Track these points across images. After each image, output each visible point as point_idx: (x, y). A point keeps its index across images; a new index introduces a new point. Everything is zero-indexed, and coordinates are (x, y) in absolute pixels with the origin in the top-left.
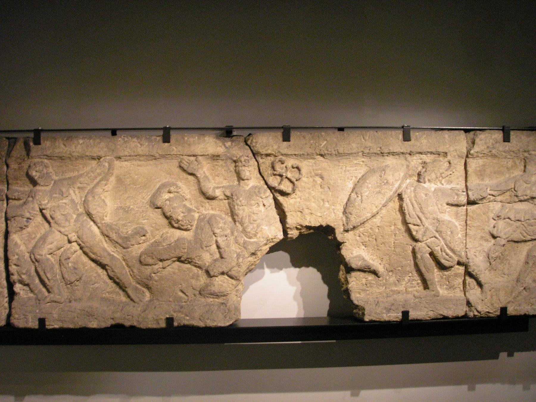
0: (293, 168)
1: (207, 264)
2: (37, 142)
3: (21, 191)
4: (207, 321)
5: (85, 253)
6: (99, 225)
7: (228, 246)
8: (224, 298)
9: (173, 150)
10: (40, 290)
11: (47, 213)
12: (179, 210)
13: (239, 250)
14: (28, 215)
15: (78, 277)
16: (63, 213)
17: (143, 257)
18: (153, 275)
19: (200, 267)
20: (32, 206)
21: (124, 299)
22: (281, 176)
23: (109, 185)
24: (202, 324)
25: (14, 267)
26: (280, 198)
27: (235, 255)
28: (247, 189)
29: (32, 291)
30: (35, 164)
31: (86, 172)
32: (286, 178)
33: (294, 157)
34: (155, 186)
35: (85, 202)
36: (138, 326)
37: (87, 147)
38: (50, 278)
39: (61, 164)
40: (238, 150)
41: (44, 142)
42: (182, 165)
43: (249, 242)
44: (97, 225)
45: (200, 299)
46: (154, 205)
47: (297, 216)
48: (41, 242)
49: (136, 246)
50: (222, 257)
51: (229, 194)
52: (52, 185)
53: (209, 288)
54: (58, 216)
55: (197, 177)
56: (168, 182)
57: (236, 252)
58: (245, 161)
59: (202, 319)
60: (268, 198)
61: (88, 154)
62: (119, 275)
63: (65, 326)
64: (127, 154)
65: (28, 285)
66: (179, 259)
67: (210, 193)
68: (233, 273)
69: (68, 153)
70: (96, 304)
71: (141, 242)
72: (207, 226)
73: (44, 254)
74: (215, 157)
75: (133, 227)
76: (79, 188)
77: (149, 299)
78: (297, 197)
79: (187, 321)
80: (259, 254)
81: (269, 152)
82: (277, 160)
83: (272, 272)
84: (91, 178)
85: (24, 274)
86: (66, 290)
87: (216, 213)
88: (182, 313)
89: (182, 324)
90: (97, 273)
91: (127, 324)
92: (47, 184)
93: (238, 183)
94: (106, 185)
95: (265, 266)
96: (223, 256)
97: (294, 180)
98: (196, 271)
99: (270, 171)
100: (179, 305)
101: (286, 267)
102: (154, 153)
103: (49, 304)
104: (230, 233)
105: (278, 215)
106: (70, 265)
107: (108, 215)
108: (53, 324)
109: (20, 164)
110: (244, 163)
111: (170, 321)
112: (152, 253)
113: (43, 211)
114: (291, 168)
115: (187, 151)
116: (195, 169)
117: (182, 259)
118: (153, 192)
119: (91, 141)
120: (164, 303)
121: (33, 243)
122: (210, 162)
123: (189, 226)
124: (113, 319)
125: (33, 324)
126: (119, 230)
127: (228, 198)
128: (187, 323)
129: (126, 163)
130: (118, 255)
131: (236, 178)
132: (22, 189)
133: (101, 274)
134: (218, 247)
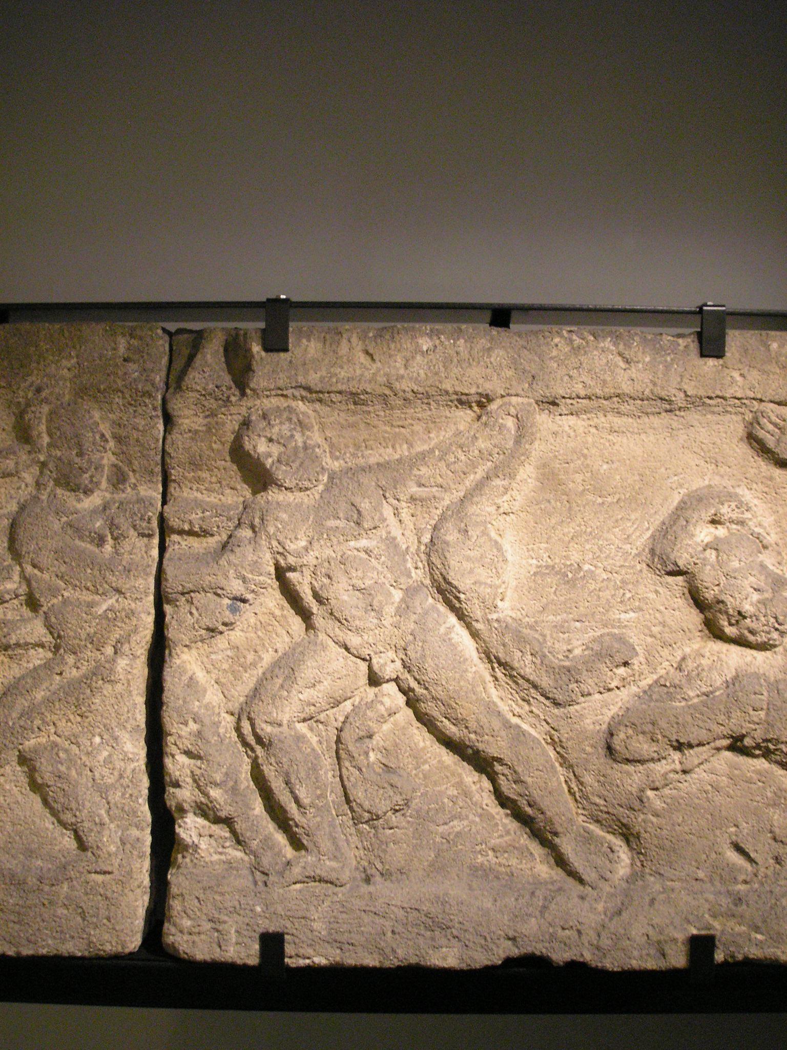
2: (276, 342)
3: (215, 507)
5: (424, 719)
9: (733, 381)
10: (267, 838)
11: (302, 582)
14: (236, 587)
16: (360, 584)
18: (650, 793)
20: (251, 557)
21: (544, 869)
25: (182, 759)
29: (239, 841)
30: (264, 416)
31: (437, 447)
34: (666, 499)
37: (447, 362)
38: (306, 801)
39: (352, 419)
41: (298, 344)
42: (761, 434)
44: (468, 626)
46: (664, 564)
48: (279, 681)
49: (597, 696)
52: (321, 488)
54: (341, 593)
56: (710, 486)
61: (447, 386)
62: (536, 794)
63: (351, 960)
64: (579, 389)
65: (227, 822)
66: (737, 745)
69: (382, 379)
70: (455, 889)
71: (613, 685)
73: (285, 718)
76: (413, 499)
85: (216, 785)
86: (354, 840)
88: (741, 919)
89: (740, 957)
90: (460, 784)
91: (560, 956)
92: (307, 484)
103: (298, 886)
106: (372, 756)
107: (509, 593)
108: (310, 951)
109: (213, 414)
111: (701, 945)
113: (290, 575)
117: (748, 742)
118: (659, 518)
119: (461, 342)
120: (677, 884)
121: (249, 680)
123: (775, 635)
124: (513, 939)
125: (243, 951)
128: (755, 953)
129: (572, 420)
130: (534, 726)
132: (213, 499)
133: (474, 788)
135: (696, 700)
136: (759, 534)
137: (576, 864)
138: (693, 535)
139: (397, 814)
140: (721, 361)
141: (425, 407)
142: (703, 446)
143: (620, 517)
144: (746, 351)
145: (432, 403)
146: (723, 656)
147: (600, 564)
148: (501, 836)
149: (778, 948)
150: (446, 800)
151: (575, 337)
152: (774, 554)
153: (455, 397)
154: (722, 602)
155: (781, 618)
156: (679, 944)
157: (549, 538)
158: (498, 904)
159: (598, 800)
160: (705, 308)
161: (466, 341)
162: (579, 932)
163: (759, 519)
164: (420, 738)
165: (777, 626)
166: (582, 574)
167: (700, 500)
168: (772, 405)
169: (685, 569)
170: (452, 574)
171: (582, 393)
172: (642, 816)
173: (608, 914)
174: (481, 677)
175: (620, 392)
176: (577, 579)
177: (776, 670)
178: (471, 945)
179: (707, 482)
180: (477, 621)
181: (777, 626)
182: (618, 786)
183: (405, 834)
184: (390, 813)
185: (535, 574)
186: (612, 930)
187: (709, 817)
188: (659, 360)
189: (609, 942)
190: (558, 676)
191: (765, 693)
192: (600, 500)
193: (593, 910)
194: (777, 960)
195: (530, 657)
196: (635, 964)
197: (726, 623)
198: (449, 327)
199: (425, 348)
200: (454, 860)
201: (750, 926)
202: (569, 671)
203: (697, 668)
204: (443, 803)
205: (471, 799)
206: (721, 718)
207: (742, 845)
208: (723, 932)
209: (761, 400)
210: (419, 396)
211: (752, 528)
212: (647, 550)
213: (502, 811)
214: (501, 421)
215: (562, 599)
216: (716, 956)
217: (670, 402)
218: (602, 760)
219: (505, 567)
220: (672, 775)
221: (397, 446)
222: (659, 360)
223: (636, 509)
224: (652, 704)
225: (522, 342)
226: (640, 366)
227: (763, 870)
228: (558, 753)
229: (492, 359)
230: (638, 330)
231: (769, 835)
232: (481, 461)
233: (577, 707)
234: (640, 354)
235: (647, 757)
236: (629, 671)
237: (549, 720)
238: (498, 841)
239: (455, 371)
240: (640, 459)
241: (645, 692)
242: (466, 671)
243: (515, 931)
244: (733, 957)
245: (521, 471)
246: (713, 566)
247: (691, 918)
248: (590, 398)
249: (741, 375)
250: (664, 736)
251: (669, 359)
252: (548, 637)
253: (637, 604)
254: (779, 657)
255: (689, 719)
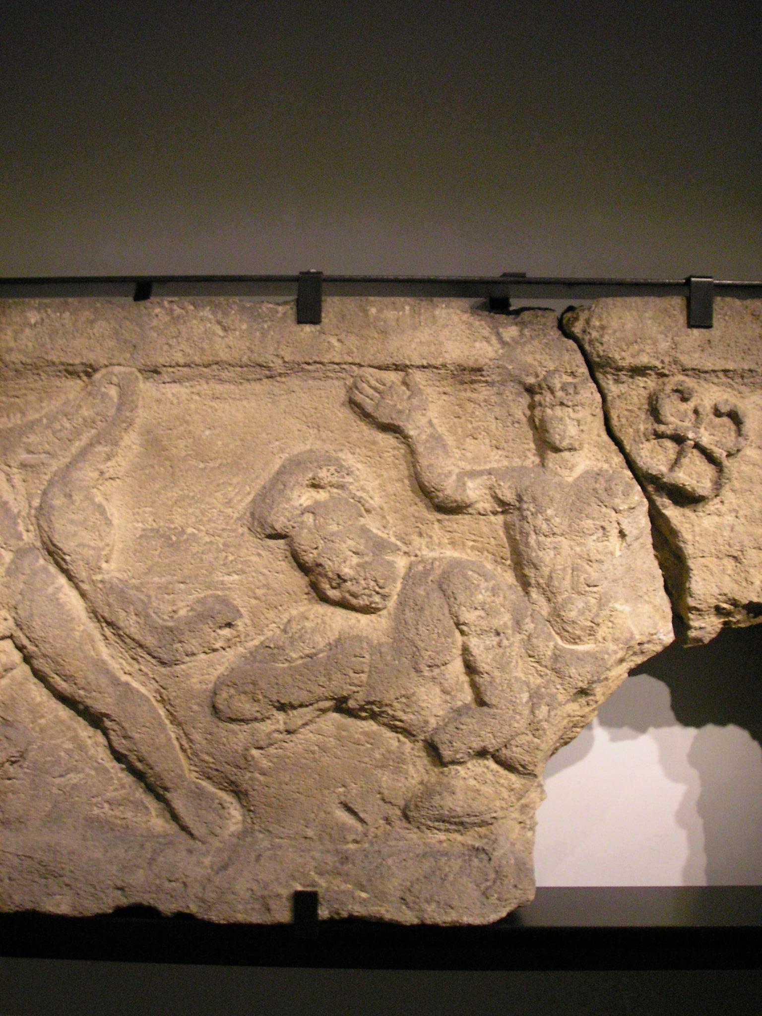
0: (718, 413)
1: (433, 722)
4: (425, 906)
5: (39, 675)
6: (85, 586)
7: (503, 668)
8: (483, 830)
9: (331, 346)
12: (346, 546)
13: (539, 681)
15: (13, 751)
17: (225, 695)
18: (255, 752)
19: (407, 732)
21: (159, 823)
22: (679, 439)
23: (119, 459)
24: (408, 917)
26: (672, 512)
27: (525, 697)
28: (570, 480)
32: (697, 446)
33: (724, 379)
34: (267, 463)
35: (42, 513)
36: (200, 916)
37: (53, 335)
40: (543, 354)
42: (359, 398)
43: (572, 652)
44: (77, 587)
45: (403, 832)
46: (262, 526)
47: (724, 571)
49: (203, 656)
50: (481, 702)
51: (509, 496)
53: (437, 800)
55: (406, 437)
56: (311, 451)
57: (527, 684)
58: (563, 389)
59: (410, 898)
60: (636, 512)
61: (53, 357)
62: (144, 749)
64: (179, 358)
66: (341, 706)
67: (449, 489)
68: (515, 753)
71: (217, 645)
72: (437, 599)
74: (468, 374)
75: (195, 595)
76: (23, 466)
77: (239, 827)
78: (723, 509)
79: (360, 904)
80: (600, 691)
81: (644, 360)
82: (668, 388)
83: (613, 739)
84: (62, 435)
87: (464, 557)
88: (346, 877)
89: (345, 914)
90: (75, 738)
91: (168, 907)
93: (537, 460)
94: (109, 458)
95: (595, 722)
96: (486, 699)
97: (720, 453)
98: (395, 743)
99: (644, 424)
100: (337, 852)
101: (658, 725)
102: (268, 357)
104: (509, 624)
105: (661, 566)
107: (115, 556)
110: (559, 394)
111: (305, 902)
112: (254, 684)
114: (712, 416)
115: (374, 351)
116: (400, 412)
117: (352, 704)
118: (261, 482)
119: (67, 314)
120: (285, 842)
122: (448, 389)
123: (377, 598)
124: (121, 889)
126: (146, 605)
127: (504, 507)
128: (359, 910)
129: (176, 388)
130: (143, 684)
131: (532, 446)
133: (89, 742)
134: (471, 669)
135: (300, 662)
136: (361, 497)
137: (186, 819)
138: (290, 499)
139: (15, 765)
140: (318, 327)
141: (36, 377)
142: (305, 411)
143: (221, 481)
144: (344, 316)
145: (42, 374)
146: (327, 619)
147: (202, 528)
148: (116, 790)
149: (381, 906)
150: (62, 754)
151: (175, 307)
152: (379, 518)
153: (61, 368)
154: (321, 565)
155: (381, 582)
156: (284, 900)
157: (154, 502)
158: (109, 854)
159: (207, 758)
160: (693, 279)
161: (71, 314)
162: (184, 883)
163: (362, 483)
164: (37, 693)
165: (377, 589)
166: (185, 537)
167: (299, 464)
168: (371, 370)
169: (284, 533)
170: (56, 536)
171: (182, 361)
172: (249, 774)
173: (215, 868)
174: (89, 635)
175: (219, 359)
176: (180, 542)
177: (380, 633)
178: (82, 893)
179: (308, 447)
180: (82, 581)
181: (377, 589)
182: (225, 745)
183: (22, 784)
184: (7, 765)
185: (141, 536)
186: (217, 883)
187: (317, 776)
188: (256, 327)
189: (214, 895)
190: (161, 636)
191: (367, 656)
192: (202, 465)
193: (199, 863)
194: (381, 919)
195: (134, 617)
196: (241, 917)
197: (328, 586)
198: (57, 301)
199: (33, 321)
200: (70, 811)
201: (355, 885)
202: (172, 631)
203: (300, 630)
204: (59, 756)
205: (86, 754)
206: (322, 680)
207: (350, 805)
208: (327, 890)
209: (360, 365)
210: (29, 367)
211: (354, 492)
212: (248, 514)
213: (117, 765)
214: (103, 390)
215: (167, 561)
216: (320, 912)
217: (269, 368)
218: (209, 719)
219: (108, 530)
220: (276, 735)
221: (12, 415)
222: (256, 327)
223: (238, 474)
224: (257, 664)
225: (125, 314)
226: (237, 333)
227: (372, 830)
228: (168, 710)
229: (95, 331)
230: (237, 299)
231: (378, 796)
232: (85, 428)
233: (183, 666)
234: (237, 322)
235: (249, 717)
236: (234, 632)
237: (158, 679)
238: (114, 794)
239: (61, 342)
240: (241, 425)
241: (251, 653)
242: (73, 629)
243: (123, 881)
244: (338, 914)
245: (126, 437)
246: (309, 530)
247: (297, 875)
248: (190, 366)
249: (339, 340)
250: (265, 697)
251: (266, 326)
252: (153, 599)
253: (240, 566)
254: (383, 621)
255: (288, 679)
